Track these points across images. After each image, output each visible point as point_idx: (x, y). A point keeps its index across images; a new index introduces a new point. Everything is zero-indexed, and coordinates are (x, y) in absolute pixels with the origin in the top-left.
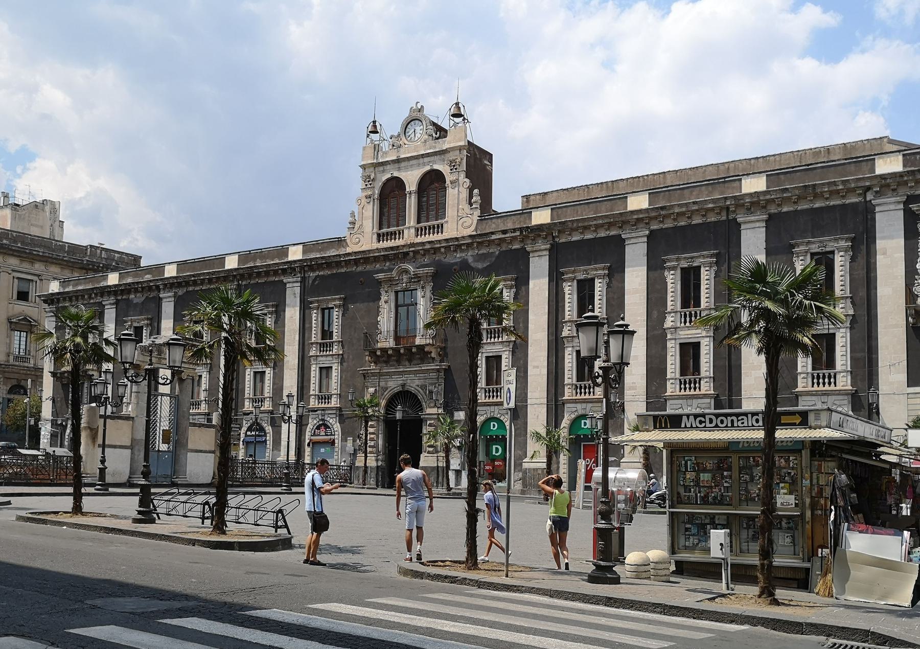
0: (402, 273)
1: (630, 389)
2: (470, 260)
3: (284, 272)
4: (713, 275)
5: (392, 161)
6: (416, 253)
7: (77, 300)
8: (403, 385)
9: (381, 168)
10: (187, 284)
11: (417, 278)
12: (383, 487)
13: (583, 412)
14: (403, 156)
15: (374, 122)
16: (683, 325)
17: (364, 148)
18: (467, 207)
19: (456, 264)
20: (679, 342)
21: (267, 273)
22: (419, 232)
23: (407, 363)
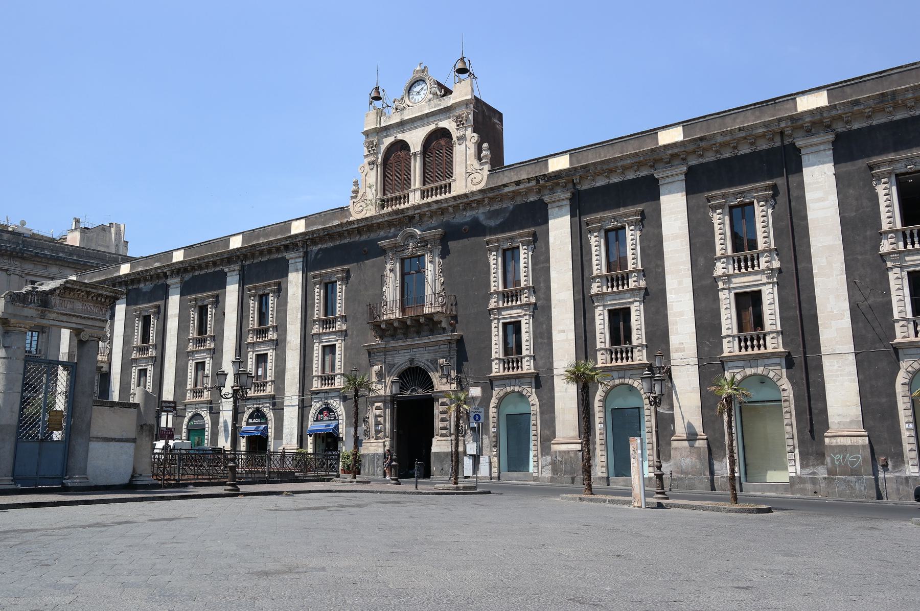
0: (407, 238)
1: (677, 351)
2: (482, 218)
3: (287, 248)
6: (422, 216)
8: (412, 361)
11: (423, 243)
16: (737, 271)
19: (466, 223)
21: (270, 251)
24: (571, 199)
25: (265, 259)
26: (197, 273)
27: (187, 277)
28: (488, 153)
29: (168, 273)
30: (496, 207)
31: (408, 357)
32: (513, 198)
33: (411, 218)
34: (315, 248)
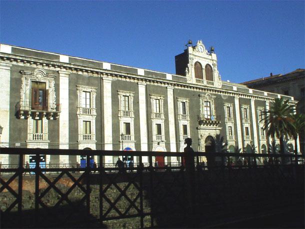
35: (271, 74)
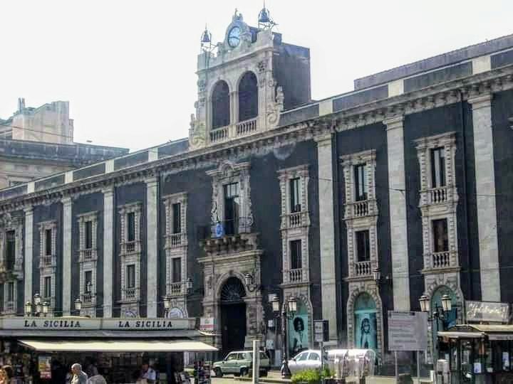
0: (226, 169)
1: (395, 267)
2: (276, 152)
3: (145, 173)
4: (454, 155)
5: (219, 66)
6: (236, 149)
7: (7, 209)
8: (231, 272)
9: (211, 74)
10: (79, 189)
11: (237, 173)
12: (181, 353)
13: (363, 290)
14: (226, 61)
15: (206, 32)
16: (433, 202)
17: (199, 56)
18: (272, 104)
19: (265, 156)
20: (430, 219)
21: (133, 176)
22: (240, 130)
23: (233, 251)
24: (332, 139)
25: (130, 182)
26: (83, 193)
27: (76, 196)
28: (282, 94)
29: (62, 193)
30: (285, 143)
31: (229, 269)
32: (295, 137)
33: (229, 151)
34: (165, 174)
35: (22, 102)
